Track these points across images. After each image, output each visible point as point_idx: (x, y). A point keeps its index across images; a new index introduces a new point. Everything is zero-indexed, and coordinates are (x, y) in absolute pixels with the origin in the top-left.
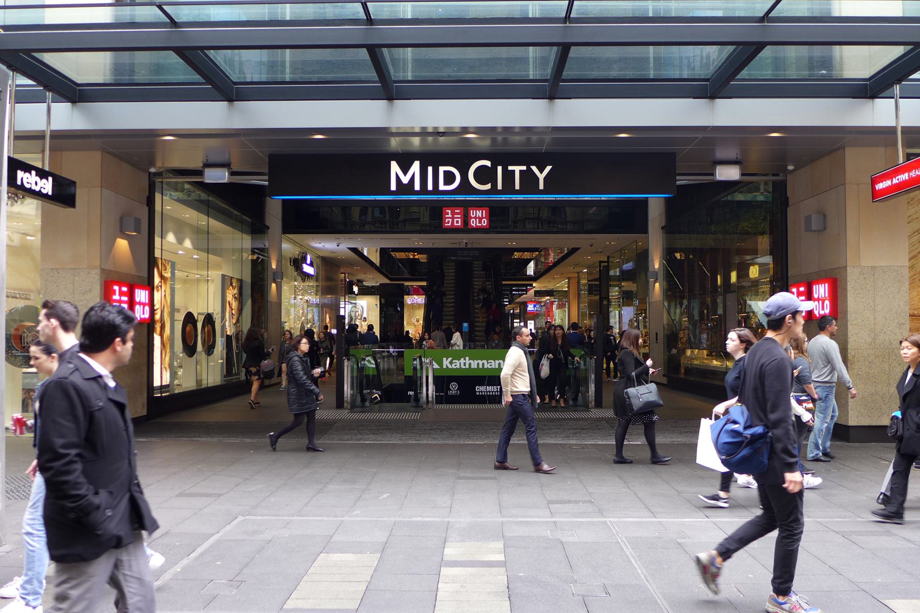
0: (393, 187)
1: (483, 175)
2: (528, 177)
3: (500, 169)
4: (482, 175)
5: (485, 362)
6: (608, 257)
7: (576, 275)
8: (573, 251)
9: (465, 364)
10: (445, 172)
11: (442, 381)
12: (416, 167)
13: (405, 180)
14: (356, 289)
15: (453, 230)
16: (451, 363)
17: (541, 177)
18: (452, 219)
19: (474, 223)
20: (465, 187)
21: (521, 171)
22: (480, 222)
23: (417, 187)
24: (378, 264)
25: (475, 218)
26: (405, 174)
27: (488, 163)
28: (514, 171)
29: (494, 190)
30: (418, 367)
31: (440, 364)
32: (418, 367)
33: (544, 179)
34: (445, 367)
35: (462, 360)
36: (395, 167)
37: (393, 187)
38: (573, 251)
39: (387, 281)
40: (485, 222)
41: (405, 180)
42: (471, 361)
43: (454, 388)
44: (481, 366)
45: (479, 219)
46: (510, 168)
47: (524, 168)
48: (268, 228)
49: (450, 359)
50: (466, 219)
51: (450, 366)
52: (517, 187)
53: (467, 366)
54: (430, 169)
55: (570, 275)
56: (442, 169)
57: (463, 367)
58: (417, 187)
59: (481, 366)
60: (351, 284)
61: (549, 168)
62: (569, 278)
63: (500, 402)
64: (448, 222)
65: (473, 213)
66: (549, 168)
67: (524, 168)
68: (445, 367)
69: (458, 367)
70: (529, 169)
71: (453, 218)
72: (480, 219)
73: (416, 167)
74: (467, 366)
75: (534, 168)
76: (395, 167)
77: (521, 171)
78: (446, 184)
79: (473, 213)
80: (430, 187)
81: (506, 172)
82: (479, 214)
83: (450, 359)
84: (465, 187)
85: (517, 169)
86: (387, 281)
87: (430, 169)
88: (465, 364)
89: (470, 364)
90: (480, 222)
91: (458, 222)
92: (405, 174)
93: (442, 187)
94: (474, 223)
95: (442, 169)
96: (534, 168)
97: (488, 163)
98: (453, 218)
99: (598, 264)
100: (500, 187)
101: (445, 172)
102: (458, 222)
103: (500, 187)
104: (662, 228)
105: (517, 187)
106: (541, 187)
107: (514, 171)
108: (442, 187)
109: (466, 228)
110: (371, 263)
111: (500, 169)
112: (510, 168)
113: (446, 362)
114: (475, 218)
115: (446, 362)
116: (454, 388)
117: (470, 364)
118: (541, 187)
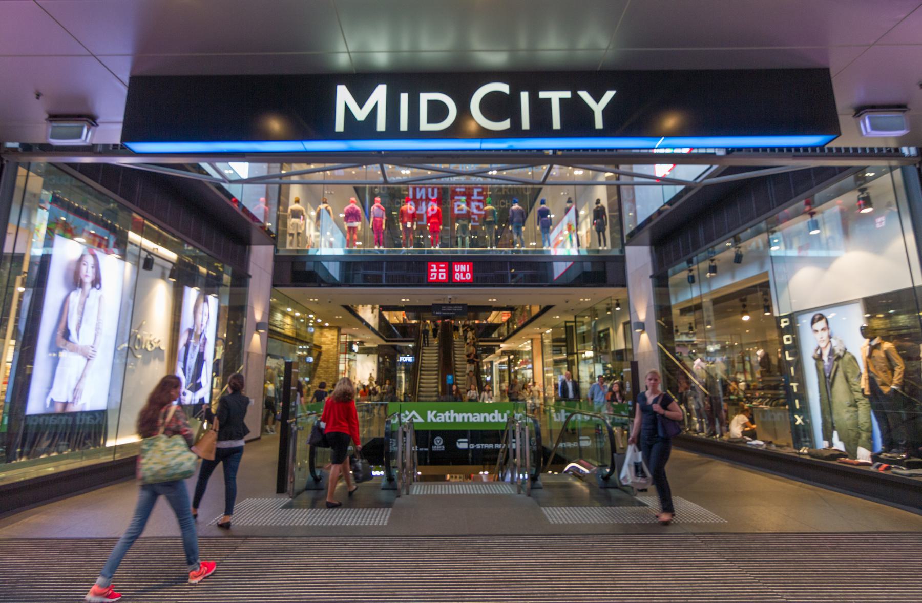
0: (340, 126)
1: (496, 107)
2: (573, 108)
3: (525, 96)
5: (470, 415)
6: (575, 317)
7: (539, 336)
9: (450, 418)
10: (431, 103)
11: (423, 437)
12: (380, 94)
13: (361, 115)
15: (438, 284)
16: (436, 416)
18: (437, 273)
19: (458, 277)
21: (562, 101)
22: (464, 276)
23: (381, 126)
24: (377, 328)
25: (460, 272)
26: (361, 105)
27: (505, 88)
28: (548, 101)
29: (515, 131)
30: (528, 272)
31: (424, 416)
32: (528, 272)
33: (605, 112)
34: (429, 420)
35: (447, 414)
36: (343, 95)
37: (340, 126)
39: (384, 343)
40: (468, 276)
41: (361, 115)
42: (456, 415)
43: (438, 444)
44: (466, 420)
45: (462, 272)
46: (543, 95)
47: (567, 94)
48: (250, 276)
49: (434, 412)
50: (450, 272)
51: (434, 420)
52: (557, 124)
53: (452, 420)
54: (404, 98)
56: (425, 98)
57: (448, 420)
58: (381, 126)
59: (466, 420)
60: (351, 343)
61: (609, 95)
62: (532, 340)
63: (380, 307)
64: (433, 276)
65: (457, 268)
66: (609, 95)
67: (567, 94)
68: (429, 420)
69: (443, 420)
70: (576, 98)
71: (438, 272)
72: (464, 273)
73: (380, 94)
74: (452, 420)
75: (584, 95)
76: (343, 95)
77: (562, 101)
78: (430, 121)
79: (457, 268)
80: (404, 126)
81: (534, 99)
82: (463, 268)
83: (434, 412)
85: (555, 97)
86: (384, 343)
87: (404, 98)
88: (450, 418)
89: (455, 418)
90: (464, 276)
91: (443, 276)
92: (361, 105)
93: (424, 126)
94: (458, 277)
95: (425, 98)
96: (584, 95)
97: (505, 88)
98: (438, 272)
99: (563, 324)
100: (526, 124)
101: (431, 103)
102: (443, 276)
103: (526, 124)
104: (651, 277)
105: (557, 124)
106: (599, 124)
107: (548, 101)
108: (424, 126)
109: (450, 282)
110: (368, 325)
111: (525, 96)
112: (543, 95)
113: (430, 416)
114: (460, 272)
115: (430, 416)
116: (438, 444)
117: (455, 418)
118: (599, 124)
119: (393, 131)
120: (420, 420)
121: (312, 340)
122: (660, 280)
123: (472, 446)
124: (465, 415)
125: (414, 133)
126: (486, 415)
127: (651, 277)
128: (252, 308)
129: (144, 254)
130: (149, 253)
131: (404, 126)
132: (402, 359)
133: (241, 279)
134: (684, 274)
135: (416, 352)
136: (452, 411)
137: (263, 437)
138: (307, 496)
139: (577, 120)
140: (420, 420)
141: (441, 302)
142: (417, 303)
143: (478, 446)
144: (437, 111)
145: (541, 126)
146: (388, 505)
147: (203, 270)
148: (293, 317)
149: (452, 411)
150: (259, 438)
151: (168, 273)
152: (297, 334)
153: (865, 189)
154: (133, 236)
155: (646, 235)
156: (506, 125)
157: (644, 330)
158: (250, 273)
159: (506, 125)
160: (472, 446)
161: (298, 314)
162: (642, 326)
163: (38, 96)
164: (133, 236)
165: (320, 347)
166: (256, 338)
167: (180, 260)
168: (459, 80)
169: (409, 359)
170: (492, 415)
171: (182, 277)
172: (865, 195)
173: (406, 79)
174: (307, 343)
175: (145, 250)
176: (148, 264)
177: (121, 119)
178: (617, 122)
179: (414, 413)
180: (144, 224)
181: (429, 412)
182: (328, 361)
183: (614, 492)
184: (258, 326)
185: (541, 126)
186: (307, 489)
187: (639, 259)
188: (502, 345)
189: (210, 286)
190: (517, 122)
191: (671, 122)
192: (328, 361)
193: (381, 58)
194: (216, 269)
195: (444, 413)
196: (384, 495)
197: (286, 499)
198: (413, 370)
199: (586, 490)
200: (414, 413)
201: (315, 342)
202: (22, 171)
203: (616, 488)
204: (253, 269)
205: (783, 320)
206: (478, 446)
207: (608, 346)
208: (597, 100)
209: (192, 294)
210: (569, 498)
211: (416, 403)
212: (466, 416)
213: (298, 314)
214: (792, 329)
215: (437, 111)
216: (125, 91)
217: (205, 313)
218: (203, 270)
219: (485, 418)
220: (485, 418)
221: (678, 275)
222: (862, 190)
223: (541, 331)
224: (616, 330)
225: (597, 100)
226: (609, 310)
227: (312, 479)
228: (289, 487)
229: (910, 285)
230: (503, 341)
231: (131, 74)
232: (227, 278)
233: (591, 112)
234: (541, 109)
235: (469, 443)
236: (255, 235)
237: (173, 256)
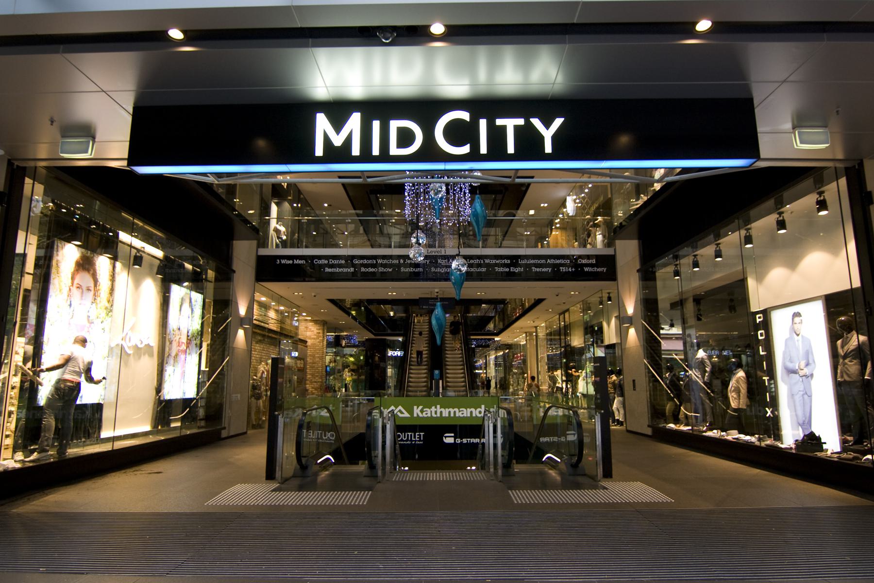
0: (319, 152)
1: (459, 133)
3: (483, 123)
4: (456, 133)
5: (456, 410)
8: (538, 302)
12: (355, 121)
14: (344, 343)
16: (422, 411)
17: (548, 134)
20: (430, 152)
21: (516, 128)
23: (356, 151)
26: (338, 130)
27: (465, 116)
28: (504, 128)
29: (474, 156)
31: (411, 412)
33: (554, 138)
36: (322, 123)
37: (319, 152)
38: (538, 302)
39: (372, 336)
42: (443, 410)
44: (452, 415)
46: (499, 122)
47: (521, 122)
48: (234, 272)
49: (421, 407)
51: (420, 415)
52: (511, 149)
53: (439, 415)
54: (376, 125)
55: (527, 330)
57: (434, 415)
58: (356, 151)
59: (452, 415)
61: (558, 122)
66: (558, 122)
67: (521, 122)
68: (415, 415)
69: (429, 415)
70: (529, 126)
73: (355, 121)
75: (536, 122)
76: (322, 123)
77: (516, 128)
80: (376, 151)
81: (491, 127)
83: (421, 407)
84: (430, 152)
85: (510, 124)
86: (372, 336)
87: (376, 125)
89: (441, 412)
92: (338, 130)
93: (394, 151)
95: (395, 125)
96: (536, 122)
97: (465, 116)
100: (484, 150)
103: (484, 150)
104: (638, 271)
105: (511, 149)
106: (548, 149)
107: (504, 128)
108: (394, 151)
111: (483, 123)
112: (499, 122)
115: (417, 411)
117: (441, 412)
118: (548, 149)
119: (366, 156)
120: (406, 415)
121: (297, 334)
122: (647, 275)
123: (458, 441)
124: (451, 409)
125: (385, 157)
126: (473, 410)
127: (638, 271)
128: (237, 304)
129: (134, 251)
130: (138, 250)
131: (376, 151)
132: (390, 353)
133: (225, 274)
134: (671, 269)
135: (404, 347)
136: (438, 406)
137: (249, 432)
138: (296, 482)
139: (530, 147)
140: (406, 415)
141: (429, 296)
142: (404, 296)
143: (465, 441)
144: (405, 138)
145: (497, 151)
146: (369, 489)
147: (189, 266)
148: (277, 311)
149: (438, 406)
150: (245, 433)
151: (155, 270)
152: (281, 328)
153: (823, 192)
154: (124, 236)
155: (634, 228)
156: (465, 149)
157: (631, 324)
158: (234, 268)
159: (465, 149)
160: (458, 441)
161: (282, 308)
162: (630, 320)
163: (52, 122)
164: (124, 236)
165: (306, 342)
166: (241, 333)
167: (166, 258)
168: (426, 109)
169: (398, 353)
170: (479, 410)
171: (169, 274)
172: (822, 198)
173: (378, 109)
174: (291, 337)
175: (134, 248)
176: (138, 260)
177: (128, 139)
178: (565, 147)
179: (400, 408)
180: (133, 223)
181: (415, 407)
182: (314, 356)
183: (580, 479)
184: (242, 322)
185: (497, 151)
186: (294, 476)
187: (628, 252)
188: (497, 339)
189: (197, 281)
190: (475, 146)
191: (624, 140)
192: (314, 356)
193: (356, 91)
194: (199, 266)
195: (430, 408)
196: (366, 481)
197: (275, 485)
198: (401, 364)
199: (558, 478)
200: (400, 408)
201: (300, 337)
202: (28, 181)
203: (585, 475)
204: (237, 265)
205: (758, 316)
206: (465, 441)
207: (602, 342)
208: (547, 126)
209: (178, 292)
210: (544, 484)
211: (405, 398)
212: (452, 410)
213: (282, 308)
214: (766, 325)
215: (405, 138)
216: (129, 119)
217: (188, 309)
218: (189, 266)
219: (471, 412)
220: (471, 412)
221: (664, 273)
222: (820, 193)
223: (535, 324)
224: (609, 324)
225: (547, 126)
226: (601, 303)
227: (298, 467)
228: (278, 474)
229: (849, 287)
230: (497, 334)
231: (135, 104)
232: (211, 274)
233: (541, 138)
234: (497, 136)
235: (455, 437)
236: (239, 227)
237: (159, 254)
